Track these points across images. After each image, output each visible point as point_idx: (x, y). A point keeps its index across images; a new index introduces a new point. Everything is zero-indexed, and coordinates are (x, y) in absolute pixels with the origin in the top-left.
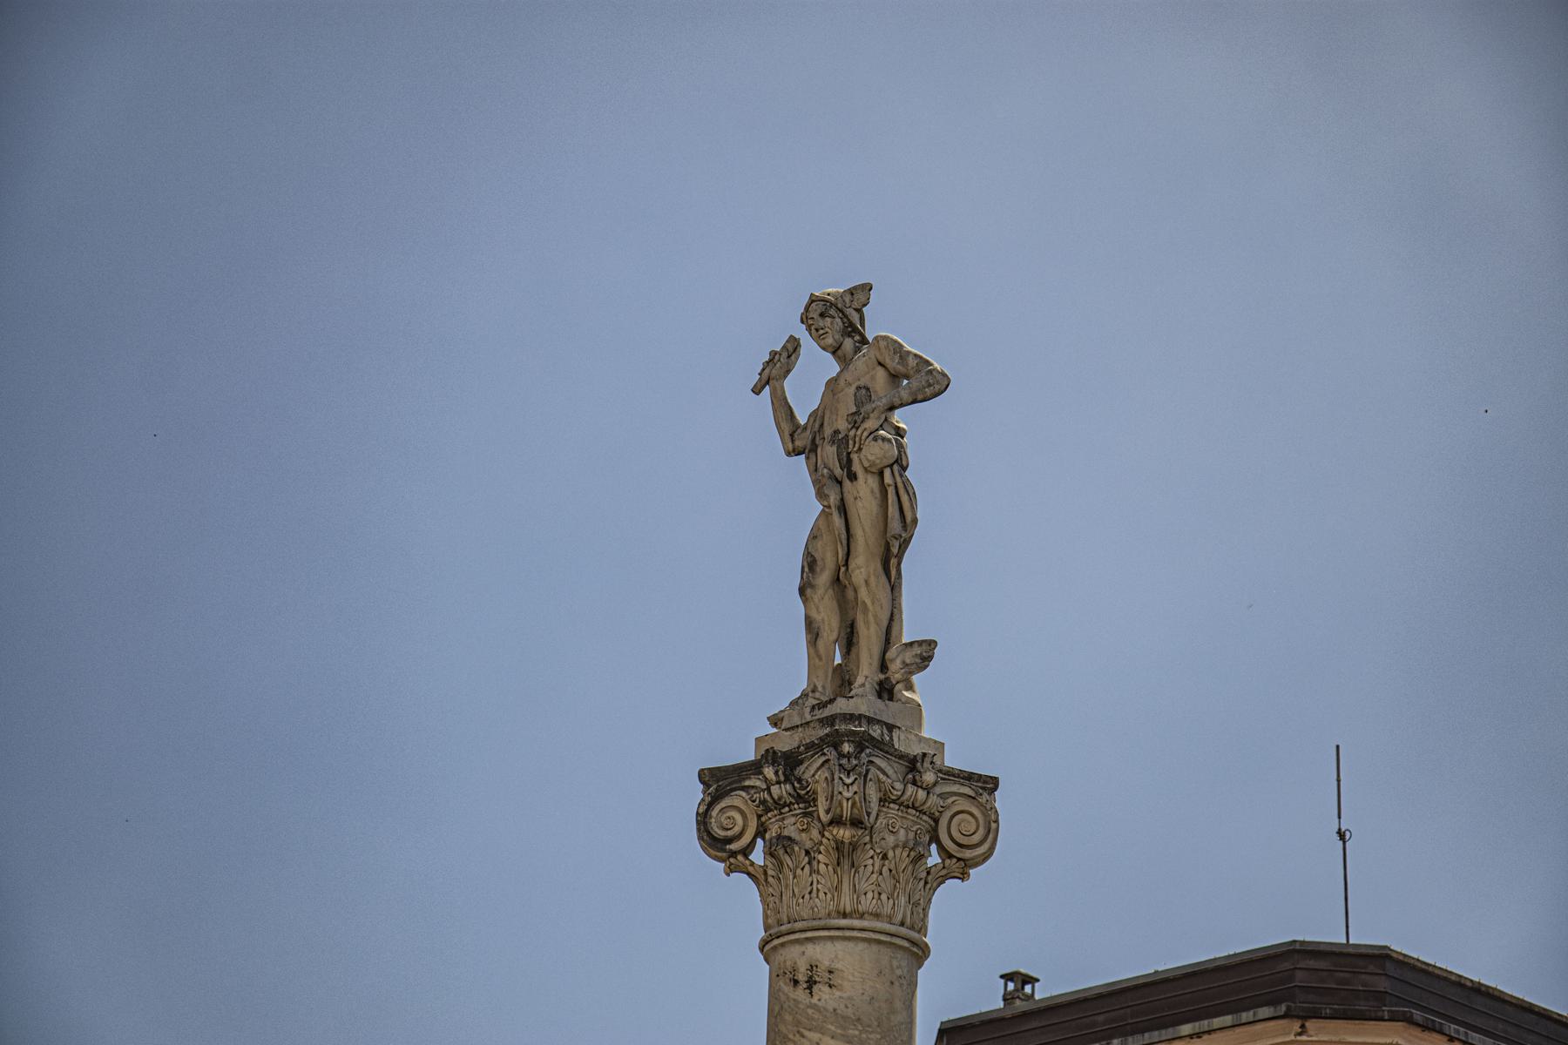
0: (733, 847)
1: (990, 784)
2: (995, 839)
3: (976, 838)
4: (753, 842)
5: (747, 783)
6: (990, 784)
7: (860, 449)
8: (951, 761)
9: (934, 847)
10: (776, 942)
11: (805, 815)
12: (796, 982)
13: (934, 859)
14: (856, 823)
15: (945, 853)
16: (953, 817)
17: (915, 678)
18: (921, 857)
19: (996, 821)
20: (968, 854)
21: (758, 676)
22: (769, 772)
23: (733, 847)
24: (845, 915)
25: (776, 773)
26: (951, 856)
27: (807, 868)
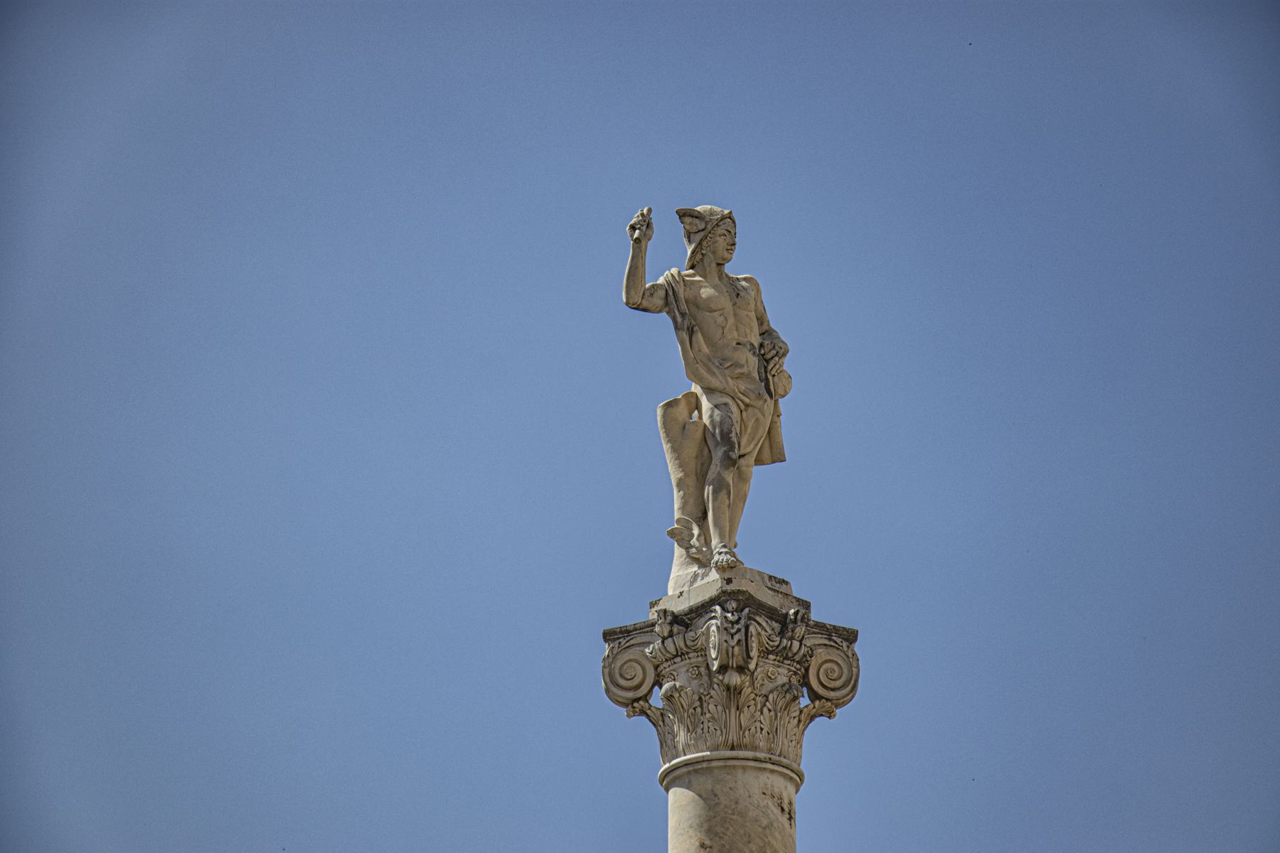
1: (851, 636)
2: (856, 681)
3: (838, 683)
4: (650, 691)
6: (851, 636)
8: (815, 616)
9: (805, 690)
10: (770, 766)
12: (783, 810)
13: (805, 701)
14: (741, 669)
15: (814, 696)
16: (827, 661)
17: (606, 649)
18: (795, 698)
19: (858, 667)
20: (832, 694)
24: (733, 748)
26: (819, 697)
27: (699, 710)
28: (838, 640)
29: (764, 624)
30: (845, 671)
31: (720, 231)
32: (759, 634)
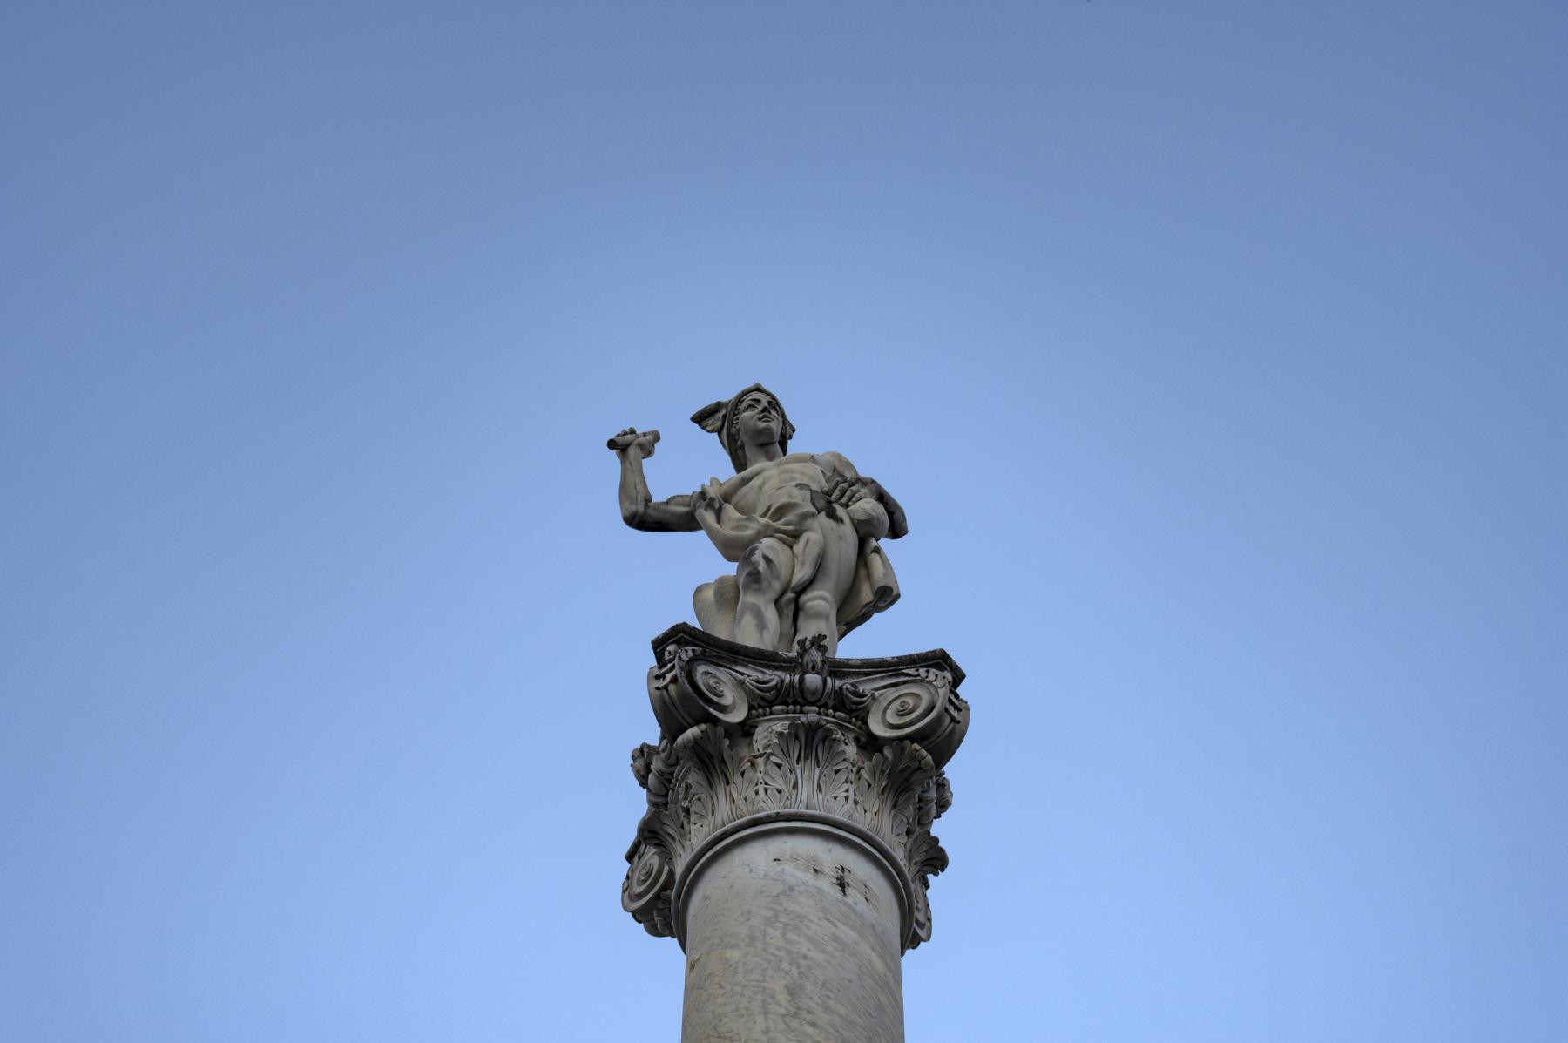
7: (847, 506)
28: (912, 671)
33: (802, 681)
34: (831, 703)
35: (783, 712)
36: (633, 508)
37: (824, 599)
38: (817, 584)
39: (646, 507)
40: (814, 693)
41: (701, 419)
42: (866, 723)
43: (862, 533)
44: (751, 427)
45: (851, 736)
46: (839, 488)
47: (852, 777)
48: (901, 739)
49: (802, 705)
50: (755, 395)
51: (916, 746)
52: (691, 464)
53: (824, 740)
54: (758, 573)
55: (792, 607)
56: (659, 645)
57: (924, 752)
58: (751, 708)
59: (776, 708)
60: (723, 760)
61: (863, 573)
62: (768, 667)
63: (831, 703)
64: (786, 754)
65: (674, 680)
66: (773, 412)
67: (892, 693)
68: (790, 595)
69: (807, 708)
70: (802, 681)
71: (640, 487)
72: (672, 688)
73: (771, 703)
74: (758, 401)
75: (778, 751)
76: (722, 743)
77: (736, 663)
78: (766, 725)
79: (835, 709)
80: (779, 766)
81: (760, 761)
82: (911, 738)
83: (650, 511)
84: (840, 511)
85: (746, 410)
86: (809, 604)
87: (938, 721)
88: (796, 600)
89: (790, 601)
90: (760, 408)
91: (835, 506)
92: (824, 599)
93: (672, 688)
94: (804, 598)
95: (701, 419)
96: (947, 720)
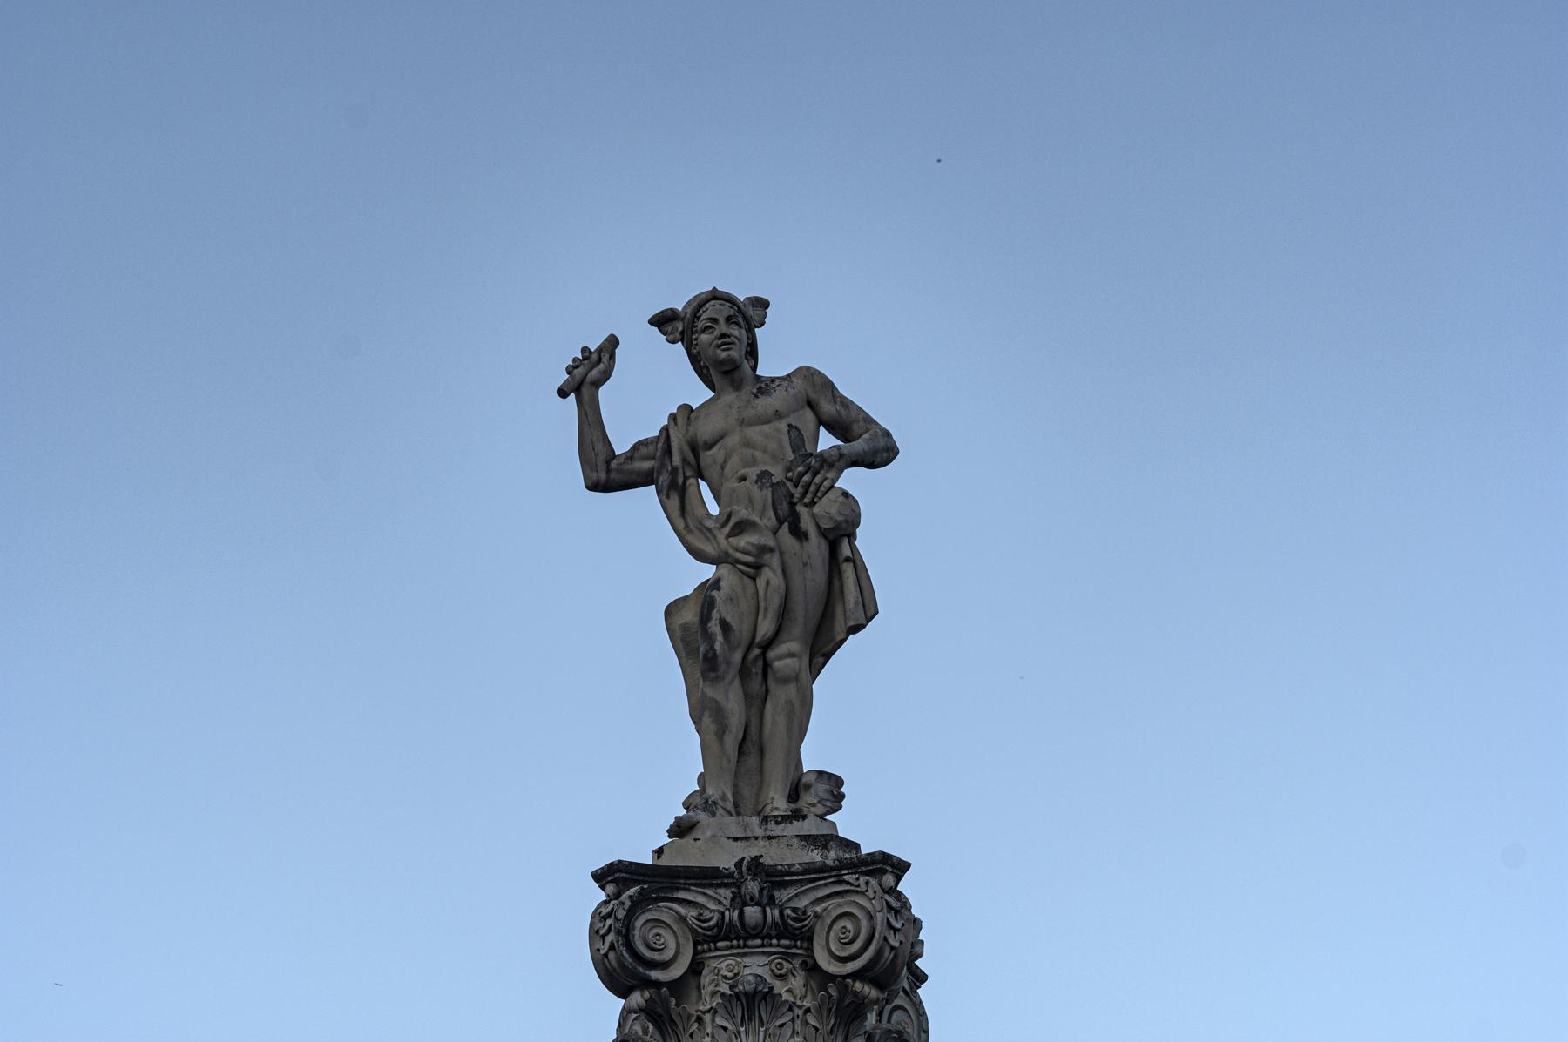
0: (655, 975)
5: (681, 895)
7: (813, 503)
11: (786, 957)
21: (643, 775)
22: (752, 887)
23: (655, 975)
25: (762, 890)
29: (700, 899)
30: (864, 923)
31: (700, 324)
32: (683, 919)
33: (741, 914)
34: (774, 933)
35: (727, 948)
36: (594, 475)
37: (791, 655)
38: (784, 636)
39: (608, 471)
40: (754, 928)
41: (663, 321)
42: (810, 940)
43: (831, 537)
44: (717, 333)
45: (797, 962)
46: (816, 395)
47: (798, 1022)
48: (845, 977)
49: (745, 939)
50: (712, 310)
51: (858, 986)
52: (654, 390)
53: (765, 998)
54: (715, 656)
55: (760, 663)
56: (601, 877)
57: (867, 989)
58: (696, 943)
59: (720, 944)
60: (671, 1019)
61: (836, 584)
62: (711, 886)
63: (774, 933)
64: (730, 1015)
65: (612, 947)
66: (735, 331)
67: (834, 907)
68: (756, 651)
69: (750, 943)
70: (741, 914)
71: (599, 446)
72: (612, 955)
73: (715, 939)
74: (715, 320)
75: (722, 1011)
76: (668, 1002)
77: (678, 889)
78: (714, 963)
79: (779, 938)
80: (725, 1029)
81: (707, 1017)
82: (856, 975)
83: (613, 475)
84: (806, 523)
85: (703, 331)
86: (777, 664)
87: (879, 954)
88: (764, 654)
89: (757, 657)
90: (717, 333)
91: (801, 509)
92: (791, 655)
93: (612, 955)
94: (771, 654)
95: (663, 321)
96: (887, 950)
